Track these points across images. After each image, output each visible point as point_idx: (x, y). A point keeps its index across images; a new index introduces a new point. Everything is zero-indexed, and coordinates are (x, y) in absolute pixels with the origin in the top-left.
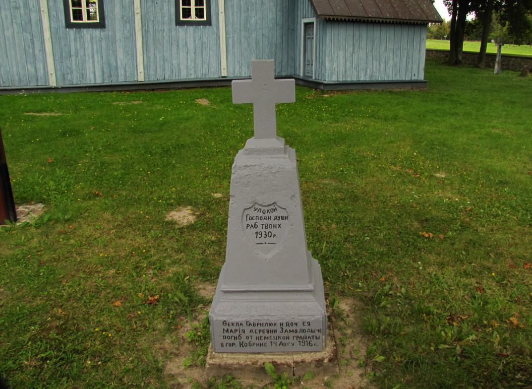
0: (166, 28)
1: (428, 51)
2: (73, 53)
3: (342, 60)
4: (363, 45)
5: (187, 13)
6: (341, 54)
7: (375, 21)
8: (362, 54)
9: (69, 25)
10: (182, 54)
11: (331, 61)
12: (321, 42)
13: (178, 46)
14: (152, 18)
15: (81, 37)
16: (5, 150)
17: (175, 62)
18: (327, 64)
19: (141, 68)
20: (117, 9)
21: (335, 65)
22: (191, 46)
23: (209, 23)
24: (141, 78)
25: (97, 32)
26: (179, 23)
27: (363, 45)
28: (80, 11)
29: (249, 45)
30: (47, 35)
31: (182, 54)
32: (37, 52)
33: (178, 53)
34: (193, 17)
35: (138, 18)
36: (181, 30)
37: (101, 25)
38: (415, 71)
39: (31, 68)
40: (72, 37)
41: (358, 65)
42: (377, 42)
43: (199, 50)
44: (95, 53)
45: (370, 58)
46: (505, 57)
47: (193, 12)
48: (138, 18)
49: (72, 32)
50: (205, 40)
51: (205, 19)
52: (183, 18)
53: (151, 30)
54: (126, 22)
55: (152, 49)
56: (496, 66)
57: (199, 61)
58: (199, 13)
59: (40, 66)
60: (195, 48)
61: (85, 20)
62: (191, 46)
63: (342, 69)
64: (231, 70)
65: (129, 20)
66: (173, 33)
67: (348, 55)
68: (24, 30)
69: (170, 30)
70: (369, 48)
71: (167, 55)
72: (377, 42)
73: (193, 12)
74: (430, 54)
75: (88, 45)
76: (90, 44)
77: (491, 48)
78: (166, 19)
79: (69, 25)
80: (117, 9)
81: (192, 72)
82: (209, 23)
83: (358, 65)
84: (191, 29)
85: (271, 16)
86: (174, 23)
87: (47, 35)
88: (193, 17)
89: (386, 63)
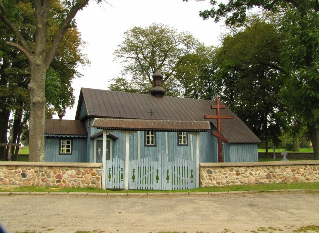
0: (175, 147)
1: (259, 153)
2: (146, 155)
5: (148, 142)
6: (234, 154)
7: (53, 137)
8: (240, 154)
9: (145, 146)
12: (228, 151)
14: (170, 143)
15: (149, 150)
18: (231, 158)
20: (160, 140)
23: (187, 145)
25: (154, 148)
27: (240, 151)
28: (149, 141)
30: (139, 149)
32: (135, 154)
33: (178, 155)
34: (183, 143)
35: (167, 143)
36: (179, 147)
37: (155, 146)
40: (146, 149)
41: (239, 158)
42: (244, 150)
43: (185, 154)
45: (242, 155)
46: (277, 153)
48: (167, 143)
49: (146, 148)
50: (186, 151)
51: (154, 144)
52: (69, 152)
54: (163, 145)
55: (170, 154)
56: (274, 157)
58: (185, 142)
60: (183, 154)
61: (150, 144)
65: (164, 144)
66: (177, 149)
67: (236, 154)
69: (176, 148)
70: (242, 152)
72: (244, 150)
75: (151, 152)
77: (270, 151)
78: (175, 144)
79: (145, 146)
82: (187, 145)
83: (239, 158)
84: (182, 147)
85: (206, 142)
87: (139, 149)
88: (150, 144)
89: (247, 156)
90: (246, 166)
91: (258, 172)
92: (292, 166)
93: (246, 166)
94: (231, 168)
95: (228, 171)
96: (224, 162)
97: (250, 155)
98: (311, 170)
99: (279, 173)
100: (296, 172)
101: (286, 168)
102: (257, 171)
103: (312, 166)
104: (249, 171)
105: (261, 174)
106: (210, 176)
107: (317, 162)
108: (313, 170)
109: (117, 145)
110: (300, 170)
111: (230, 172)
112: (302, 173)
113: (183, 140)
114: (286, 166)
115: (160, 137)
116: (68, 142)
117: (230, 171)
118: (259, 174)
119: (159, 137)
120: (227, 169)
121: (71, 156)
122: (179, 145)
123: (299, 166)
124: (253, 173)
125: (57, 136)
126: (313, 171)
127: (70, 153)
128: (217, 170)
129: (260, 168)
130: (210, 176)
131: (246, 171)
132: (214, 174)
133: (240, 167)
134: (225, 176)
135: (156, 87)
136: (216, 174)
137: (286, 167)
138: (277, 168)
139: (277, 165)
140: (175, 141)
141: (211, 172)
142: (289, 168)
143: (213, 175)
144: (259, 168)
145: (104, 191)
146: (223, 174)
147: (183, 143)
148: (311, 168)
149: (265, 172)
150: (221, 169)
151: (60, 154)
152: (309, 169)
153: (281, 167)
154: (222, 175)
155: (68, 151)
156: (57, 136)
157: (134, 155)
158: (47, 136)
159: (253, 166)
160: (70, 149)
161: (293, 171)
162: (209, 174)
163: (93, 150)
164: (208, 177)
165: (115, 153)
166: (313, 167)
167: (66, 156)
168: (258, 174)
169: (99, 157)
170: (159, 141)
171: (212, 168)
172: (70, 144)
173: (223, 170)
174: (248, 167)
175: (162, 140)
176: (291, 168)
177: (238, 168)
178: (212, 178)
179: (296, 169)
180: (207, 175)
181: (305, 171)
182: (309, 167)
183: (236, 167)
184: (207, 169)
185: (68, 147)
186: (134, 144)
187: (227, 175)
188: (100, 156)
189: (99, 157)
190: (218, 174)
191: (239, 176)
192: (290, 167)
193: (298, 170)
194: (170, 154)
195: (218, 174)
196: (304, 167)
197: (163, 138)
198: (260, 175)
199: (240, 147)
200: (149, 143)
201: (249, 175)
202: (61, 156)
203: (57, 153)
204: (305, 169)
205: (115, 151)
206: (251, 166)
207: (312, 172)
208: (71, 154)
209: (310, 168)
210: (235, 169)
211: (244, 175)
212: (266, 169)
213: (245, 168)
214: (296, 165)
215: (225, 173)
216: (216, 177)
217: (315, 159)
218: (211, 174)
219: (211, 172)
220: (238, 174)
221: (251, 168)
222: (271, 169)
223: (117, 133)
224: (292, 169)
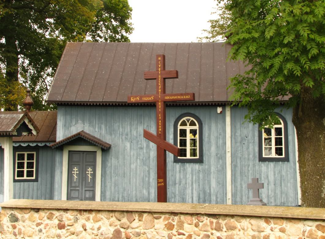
0: (251, 164)
2: (177, 181)
14: (239, 155)
15: (184, 170)
19: (229, 195)
20: (213, 149)
25: (197, 166)
28: (276, 144)
34: (273, 155)
35: (228, 155)
36: (264, 166)
37: (200, 161)
40: (178, 170)
43: (278, 182)
44: (194, 182)
48: (228, 155)
51: (198, 157)
52: (33, 176)
53: (239, 165)
57: (278, 192)
62: (271, 178)
65: (221, 157)
66: (257, 167)
69: (254, 165)
75: (189, 176)
76: (190, 175)
78: (251, 156)
80: (213, 149)
82: (287, 159)
84: (272, 164)
86: (257, 159)
88: (188, 156)
90: (77, 210)
91: (97, 225)
92: (167, 216)
93: (77, 210)
94: (49, 212)
95: (46, 218)
98: (209, 229)
99: (137, 230)
100: (174, 232)
101: (156, 220)
102: (96, 221)
103: (212, 220)
104: (82, 219)
105: (103, 229)
106: (14, 227)
107: (320, 213)
108: (216, 229)
109: (112, 161)
110: (186, 225)
111: (48, 221)
112: (187, 234)
114: (155, 216)
115: (213, 141)
116: (30, 157)
117: (48, 218)
118: (99, 229)
119: (209, 142)
120: (42, 214)
121: (35, 183)
122: (262, 159)
123: (182, 217)
124: (89, 225)
125: (29, 145)
126: (214, 231)
127: (34, 178)
128: (27, 216)
130: (14, 227)
131: (77, 220)
132: (20, 223)
133: (66, 210)
134: (37, 229)
136: (24, 224)
137: (155, 218)
138: (136, 216)
139: (137, 212)
141: (17, 220)
142: (161, 220)
143: (19, 225)
144: (100, 215)
146: (35, 223)
147: (273, 155)
148: (212, 223)
149: (110, 225)
150: (32, 212)
152: (205, 225)
153: (145, 215)
154: (33, 227)
155: (30, 174)
156: (29, 145)
157: (149, 183)
158: (17, 145)
159: (90, 211)
160: (34, 169)
161: (170, 227)
162: (12, 222)
163: (62, 172)
164: (11, 229)
165: (108, 177)
166: (215, 221)
167: (26, 183)
168: (96, 229)
169: (75, 187)
170: (211, 150)
171: (19, 211)
172: (35, 161)
173: (36, 215)
174: (80, 211)
175: (217, 147)
176: (164, 220)
177: (62, 213)
178: (16, 231)
179: (175, 223)
180: (9, 224)
181: (196, 229)
182: (206, 220)
183: (58, 210)
184: (10, 212)
185: (30, 165)
186: (149, 157)
187: (42, 227)
188: (91, 185)
189: (75, 187)
190: (27, 222)
191: (63, 230)
192: (163, 216)
193: (181, 225)
194: (239, 180)
195: (27, 222)
196: (194, 220)
197: (221, 142)
198: (100, 231)
201: (82, 229)
204: (197, 226)
205: (108, 172)
206: (85, 211)
207: (212, 234)
208: (36, 180)
209: (209, 223)
210: (57, 214)
211: (72, 229)
212: (113, 219)
213: (75, 213)
215: (39, 221)
216: (23, 229)
217: (316, 206)
218: (16, 223)
219: (17, 220)
220: (61, 226)
221: (86, 215)
222: (125, 220)
224: (166, 222)
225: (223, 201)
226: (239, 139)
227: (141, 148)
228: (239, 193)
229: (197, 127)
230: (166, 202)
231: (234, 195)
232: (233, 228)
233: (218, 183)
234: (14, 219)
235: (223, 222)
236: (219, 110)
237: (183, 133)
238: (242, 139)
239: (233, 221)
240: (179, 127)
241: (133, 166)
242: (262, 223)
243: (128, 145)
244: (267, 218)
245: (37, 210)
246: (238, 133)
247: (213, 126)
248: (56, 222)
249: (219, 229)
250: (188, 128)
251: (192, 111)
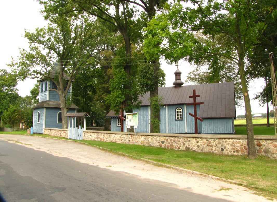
0: (173, 121)
3: (206, 128)
4: (212, 124)
5: (178, 118)
10: (177, 127)
11: (204, 128)
13: (176, 125)
16: (48, 152)
17: (175, 129)
19: (167, 130)
20: (163, 117)
21: (205, 129)
22: (178, 125)
24: (186, 132)
26: (176, 120)
27: (212, 124)
28: (180, 116)
29: (192, 125)
31: (177, 127)
34: (179, 119)
36: (176, 122)
38: (229, 131)
39: (146, 129)
43: (180, 126)
47: (179, 118)
52: (59, 122)
53: (170, 122)
57: (180, 129)
58: (181, 118)
59: (147, 129)
62: (178, 125)
63: (207, 130)
64: (188, 131)
65: (165, 120)
68: (145, 122)
71: (173, 127)
73: (179, 118)
74: (157, 130)
80: (163, 117)
81: (179, 131)
82: (183, 120)
84: (179, 121)
88: (179, 119)
89: (220, 128)
96: (7, 131)
97: (223, 127)
113: (179, 116)
119: (162, 115)
120: (88, 133)
129: (95, 133)
135: (178, 80)
140: (173, 117)
143: (85, 135)
145: (69, 139)
151: (117, 126)
182: (108, 134)
193: (105, 135)
197: (165, 115)
199: (208, 121)
200: (178, 118)
202: (118, 127)
203: (116, 126)
208: (117, 126)
214: (104, 133)
223: (10, 129)
225: (148, 132)
226: (170, 114)
227: (145, 118)
228: (170, 130)
229: (181, 111)
230: (159, 133)
231: (168, 130)
232: (111, 136)
233: (164, 126)
234: (85, 134)
235: (110, 135)
236: (165, 107)
237: (178, 112)
238: (171, 115)
239: (111, 134)
240: (177, 111)
241: (143, 122)
242: (115, 135)
243: (141, 117)
244: (115, 134)
245: (87, 132)
246: (170, 113)
247: (163, 111)
248: (90, 135)
249: (109, 136)
250: (179, 111)
251: (180, 106)
